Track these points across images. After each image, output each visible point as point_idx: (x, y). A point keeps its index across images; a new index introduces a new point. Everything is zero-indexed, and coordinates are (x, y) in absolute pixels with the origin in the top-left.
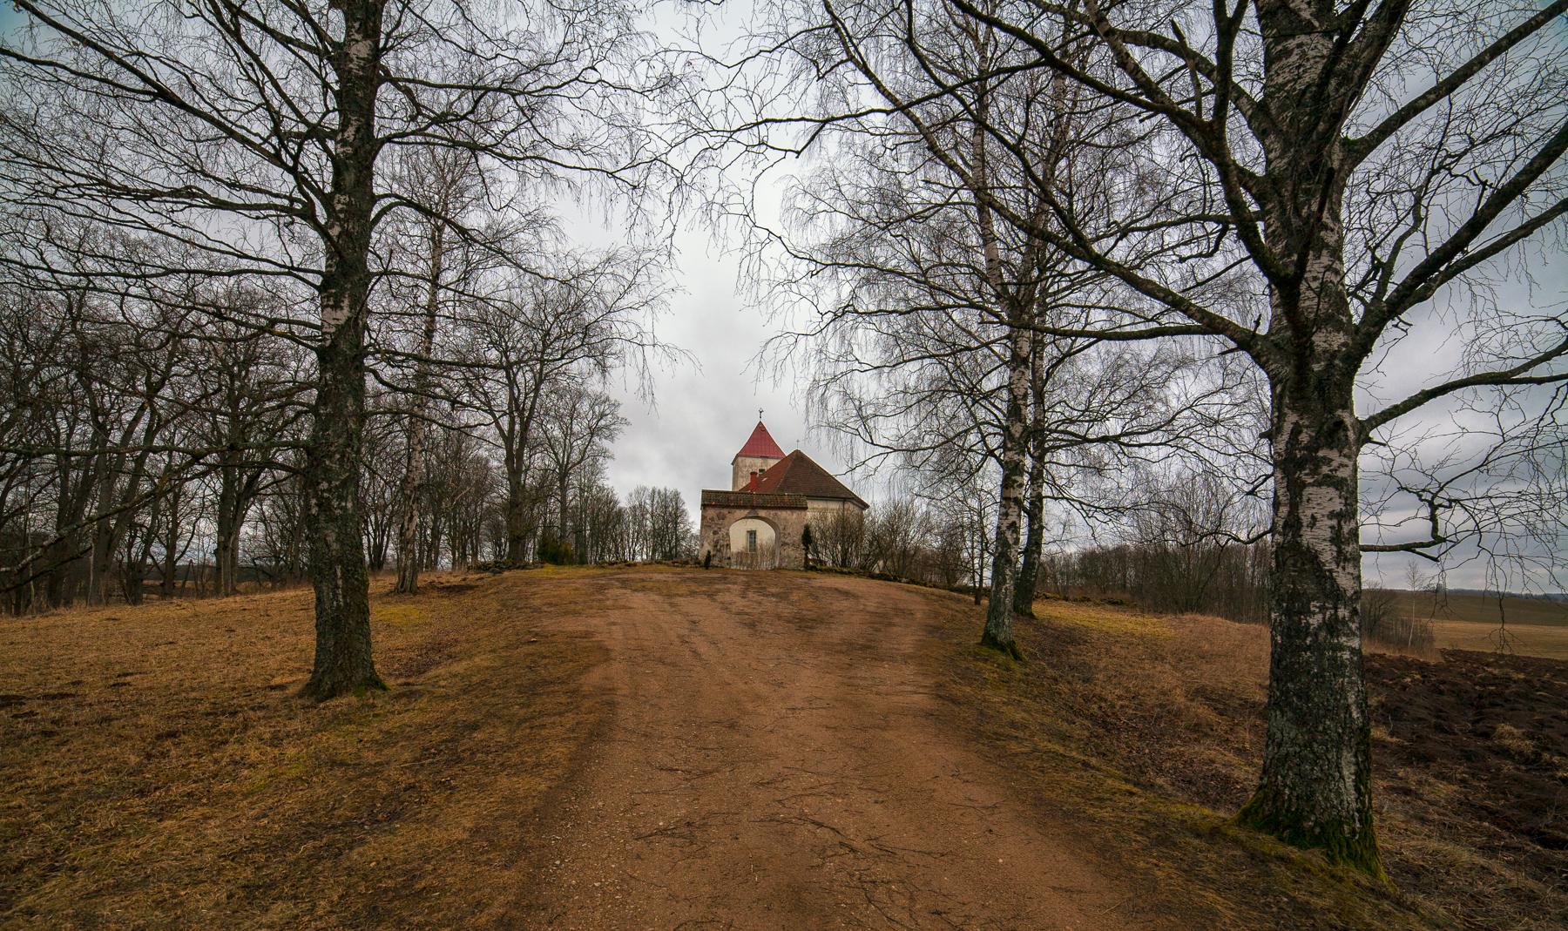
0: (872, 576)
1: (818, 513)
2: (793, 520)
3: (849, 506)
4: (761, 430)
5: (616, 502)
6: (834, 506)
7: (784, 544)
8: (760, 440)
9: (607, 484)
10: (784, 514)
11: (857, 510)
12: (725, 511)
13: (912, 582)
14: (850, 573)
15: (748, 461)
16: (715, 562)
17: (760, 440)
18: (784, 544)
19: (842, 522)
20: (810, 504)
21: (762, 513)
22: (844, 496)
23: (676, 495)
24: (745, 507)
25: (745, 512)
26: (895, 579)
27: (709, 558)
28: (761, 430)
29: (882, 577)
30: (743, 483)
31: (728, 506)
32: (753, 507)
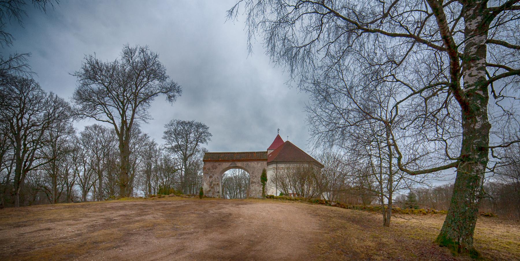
12: (217, 164)
21: (239, 164)
24: (228, 161)
32: (233, 161)
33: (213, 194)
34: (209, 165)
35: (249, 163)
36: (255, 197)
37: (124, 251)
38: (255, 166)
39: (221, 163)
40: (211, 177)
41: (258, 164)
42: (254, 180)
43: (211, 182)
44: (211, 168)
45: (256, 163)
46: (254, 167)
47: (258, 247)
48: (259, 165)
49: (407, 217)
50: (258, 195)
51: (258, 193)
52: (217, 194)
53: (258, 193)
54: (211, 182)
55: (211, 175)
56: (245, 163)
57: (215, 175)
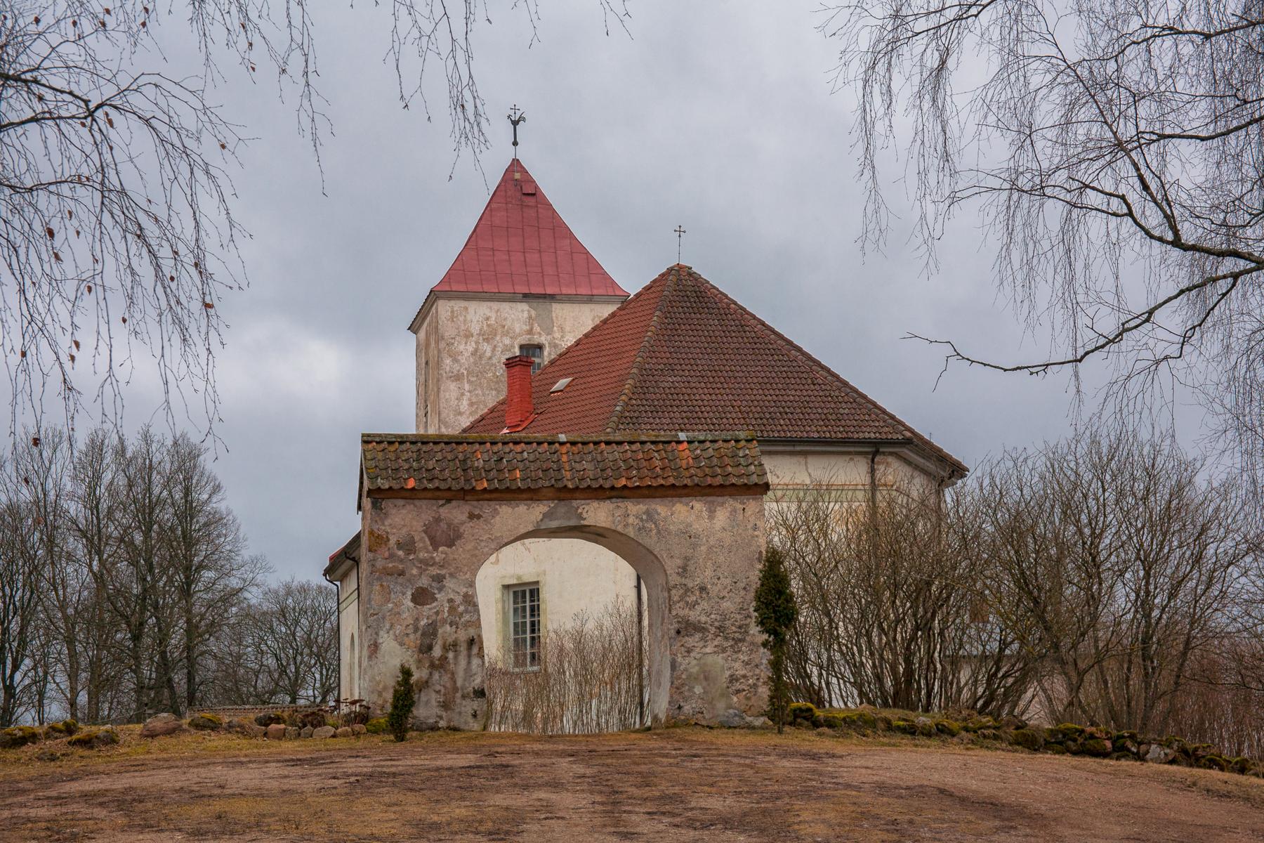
0: (1029, 741)
1: (812, 500)
2: (718, 539)
3: (893, 472)
4: (518, 194)
5: (1187, 470)
6: (848, 473)
7: (686, 628)
8: (520, 234)
9: (275, 580)
10: (684, 514)
11: (918, 486)
12: (456, 513)
13: (1189, 757)
14: (942, 732)
15: (478, 314)
16: (426, 709)
17: (520, 234)
18: (686, 628)
19: (881, 537)
20: (783, 472)
21: (598, 513)
22: (879, 438)
23: (186, 461)
24: (529, 494)
25: (531, 513)
26: (1120, 750)
27: (405, 694)
28: (518, 194)
29: (1065, 741)
30: (461, 410)
31: (466, 494)
32: (564, 493)
33: (445, 706)
34: (405, 520)
35: (661, 508)
36: (707, 717)
37: (518, 839)
38: (697, 527)
39: (486, 508)
40: (421, 597)
41: (712, 513)
42: (694, 615)
43: (430, 632)
44: (422, 541)
45: (698, 505)
46: (690, 536)
47: (590, 625)
48: (722, 516)
49: (81, 782)
50: (721, 705)
51: (725, 695)
52: (476, 704)
53: (725, 695)
54: (430, 632)
55: (424, 582)
56: (635, 509)
57: (449, 583)
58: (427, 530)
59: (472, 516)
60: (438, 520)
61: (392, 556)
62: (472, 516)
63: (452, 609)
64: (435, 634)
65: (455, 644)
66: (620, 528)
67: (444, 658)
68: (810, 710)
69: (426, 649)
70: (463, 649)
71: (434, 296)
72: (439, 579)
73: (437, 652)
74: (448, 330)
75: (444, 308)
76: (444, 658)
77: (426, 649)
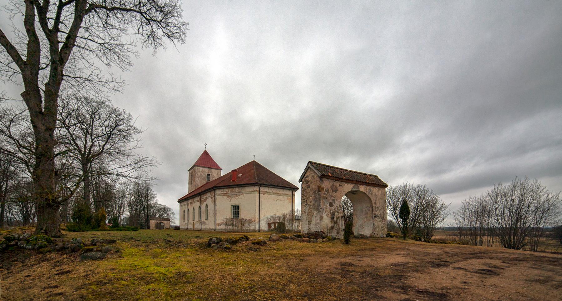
4: (206, 154)
12: (337, 184)
15: (201, 169)
28: (206, 154)
39: (343, 184)
40: (331, 205)
43: (333, 214)
55: (331, 201)
57: (336, 202)
58: (331, 188)
59: (340, 185)
60: (333, 185)
61: (325, 194)
62: (340, 185)
63: (337, 208)
64: (334, 214)
65: (339, 217)
66: (367, 193)
67: (337, 221)
68: (130, 204)
69: (333, 218)
70: (340, 218)
71: (194, 166)
72: (334, 200)
73: (335, 219)
74: (197, 171)
75: (196, 168)
76: (337, 221)
77: (333, 218)
